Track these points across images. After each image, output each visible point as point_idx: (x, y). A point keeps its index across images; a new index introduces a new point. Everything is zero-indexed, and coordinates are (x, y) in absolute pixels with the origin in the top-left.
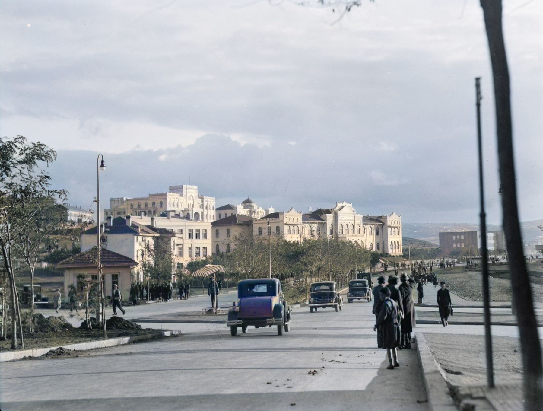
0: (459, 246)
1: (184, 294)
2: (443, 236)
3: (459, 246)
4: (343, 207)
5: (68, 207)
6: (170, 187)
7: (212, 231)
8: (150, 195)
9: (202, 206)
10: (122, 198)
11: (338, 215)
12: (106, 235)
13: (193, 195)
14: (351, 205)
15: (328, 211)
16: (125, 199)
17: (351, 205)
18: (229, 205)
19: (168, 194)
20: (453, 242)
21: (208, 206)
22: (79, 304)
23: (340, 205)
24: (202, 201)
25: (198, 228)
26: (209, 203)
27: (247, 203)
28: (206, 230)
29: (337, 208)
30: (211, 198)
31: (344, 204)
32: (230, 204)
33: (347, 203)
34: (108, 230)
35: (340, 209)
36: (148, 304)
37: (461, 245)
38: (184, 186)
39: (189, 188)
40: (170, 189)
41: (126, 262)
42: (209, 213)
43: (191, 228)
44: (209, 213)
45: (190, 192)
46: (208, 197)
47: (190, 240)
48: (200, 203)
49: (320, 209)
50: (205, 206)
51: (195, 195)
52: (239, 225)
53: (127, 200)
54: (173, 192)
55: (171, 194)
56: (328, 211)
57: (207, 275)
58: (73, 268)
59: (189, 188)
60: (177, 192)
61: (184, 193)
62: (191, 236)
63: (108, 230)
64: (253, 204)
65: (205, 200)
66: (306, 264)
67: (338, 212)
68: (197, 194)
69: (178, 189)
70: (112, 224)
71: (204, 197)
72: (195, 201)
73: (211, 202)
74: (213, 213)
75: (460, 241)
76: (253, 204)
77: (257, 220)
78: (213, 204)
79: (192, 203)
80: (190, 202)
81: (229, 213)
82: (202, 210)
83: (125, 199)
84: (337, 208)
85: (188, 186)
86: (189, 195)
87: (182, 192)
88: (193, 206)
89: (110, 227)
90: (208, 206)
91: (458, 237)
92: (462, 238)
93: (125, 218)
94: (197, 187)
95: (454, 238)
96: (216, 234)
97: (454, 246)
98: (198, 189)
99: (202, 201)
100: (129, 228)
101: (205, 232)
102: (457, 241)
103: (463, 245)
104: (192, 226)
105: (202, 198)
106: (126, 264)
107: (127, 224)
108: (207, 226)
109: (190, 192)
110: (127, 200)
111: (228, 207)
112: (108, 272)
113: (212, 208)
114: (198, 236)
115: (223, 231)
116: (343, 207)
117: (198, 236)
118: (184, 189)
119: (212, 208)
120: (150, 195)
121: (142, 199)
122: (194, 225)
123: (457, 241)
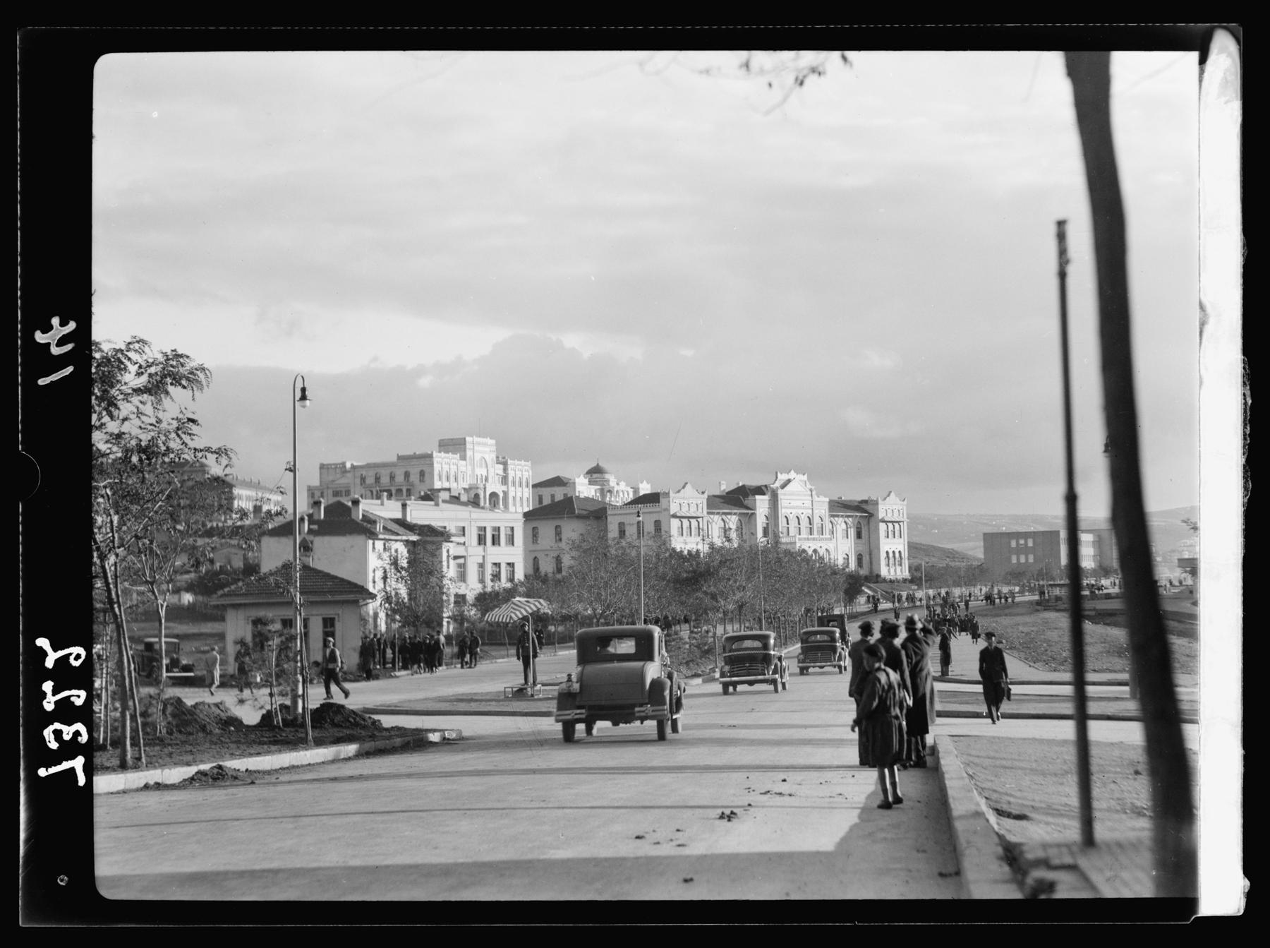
1: (467, 658)
2: (994, 540)
3: (1023, 560)
4: (789, 481)
5: (234, 482)
8: (399, 458)
9: (504, 480)
10: (344, 464)
11: (780, 497)
12: (310, 538)
13: (487, 457)
14: (805, 477)
15: (760, 490)
17: (805, 477)
18: (558, 478)
19: (435, 454)
20: (1011, 551)
23: (783, 477)
24: (505, 470)
26: (519, 474)
27: (596, 473)
29: (777, 484)
30: (523, 463)
31: (792, 475)
32: (561, 475)
34: (315, 527)
35: (783, 487)
37: (1018, 559)
39: (479, 444)
41: (351, 592)
42: (519, 494)
43: (483, 525)
44: (519, 494)
47: (481, 548)
48: (501, 472)
50: (510, 479)
51: (491, 457)
52: (579, 517)
54: (447, 452)
55: (443, 454)
56: (760, 490)
59: (479, 444)
60: (454, 452)
61: (469, 453)
62: (481, 540)
63: (315, 527)
64: (607, 476)
65: (510, 467)
67: (780, 491)
68: (494, 456)
69: (455, 445)
72: (491, 470)
73: (522, 471)
74: (527, 493)
75: (1026, 550)
76: (607, 476)
77: (615, 507)
78: (526, 475)
79: (484, 474)
80: (481, 472)
81: (559, 494)
82: (504, 488)
83: (348, 465)
85: (477, 439)
86: (478, 457)
87: (465, 450)
88: (487, 480)
89: (318, 522)
91: (1022, 542)
92: (1030, 544)
93: (350, 504)
94: (493, 442)
95: (1013, 544)
96: (534, 535)
97: (1014, 560)
98: (497, 444)
99: (505, 470)
102: (1018, 551)
104: (485, 520)
105: (505, 464)
107: (353, 516)
111: (557, 482)
114: (496, 541)
116: (789, 481)
118: (468, 446)
120: (399, 458)
121: (384, 465)
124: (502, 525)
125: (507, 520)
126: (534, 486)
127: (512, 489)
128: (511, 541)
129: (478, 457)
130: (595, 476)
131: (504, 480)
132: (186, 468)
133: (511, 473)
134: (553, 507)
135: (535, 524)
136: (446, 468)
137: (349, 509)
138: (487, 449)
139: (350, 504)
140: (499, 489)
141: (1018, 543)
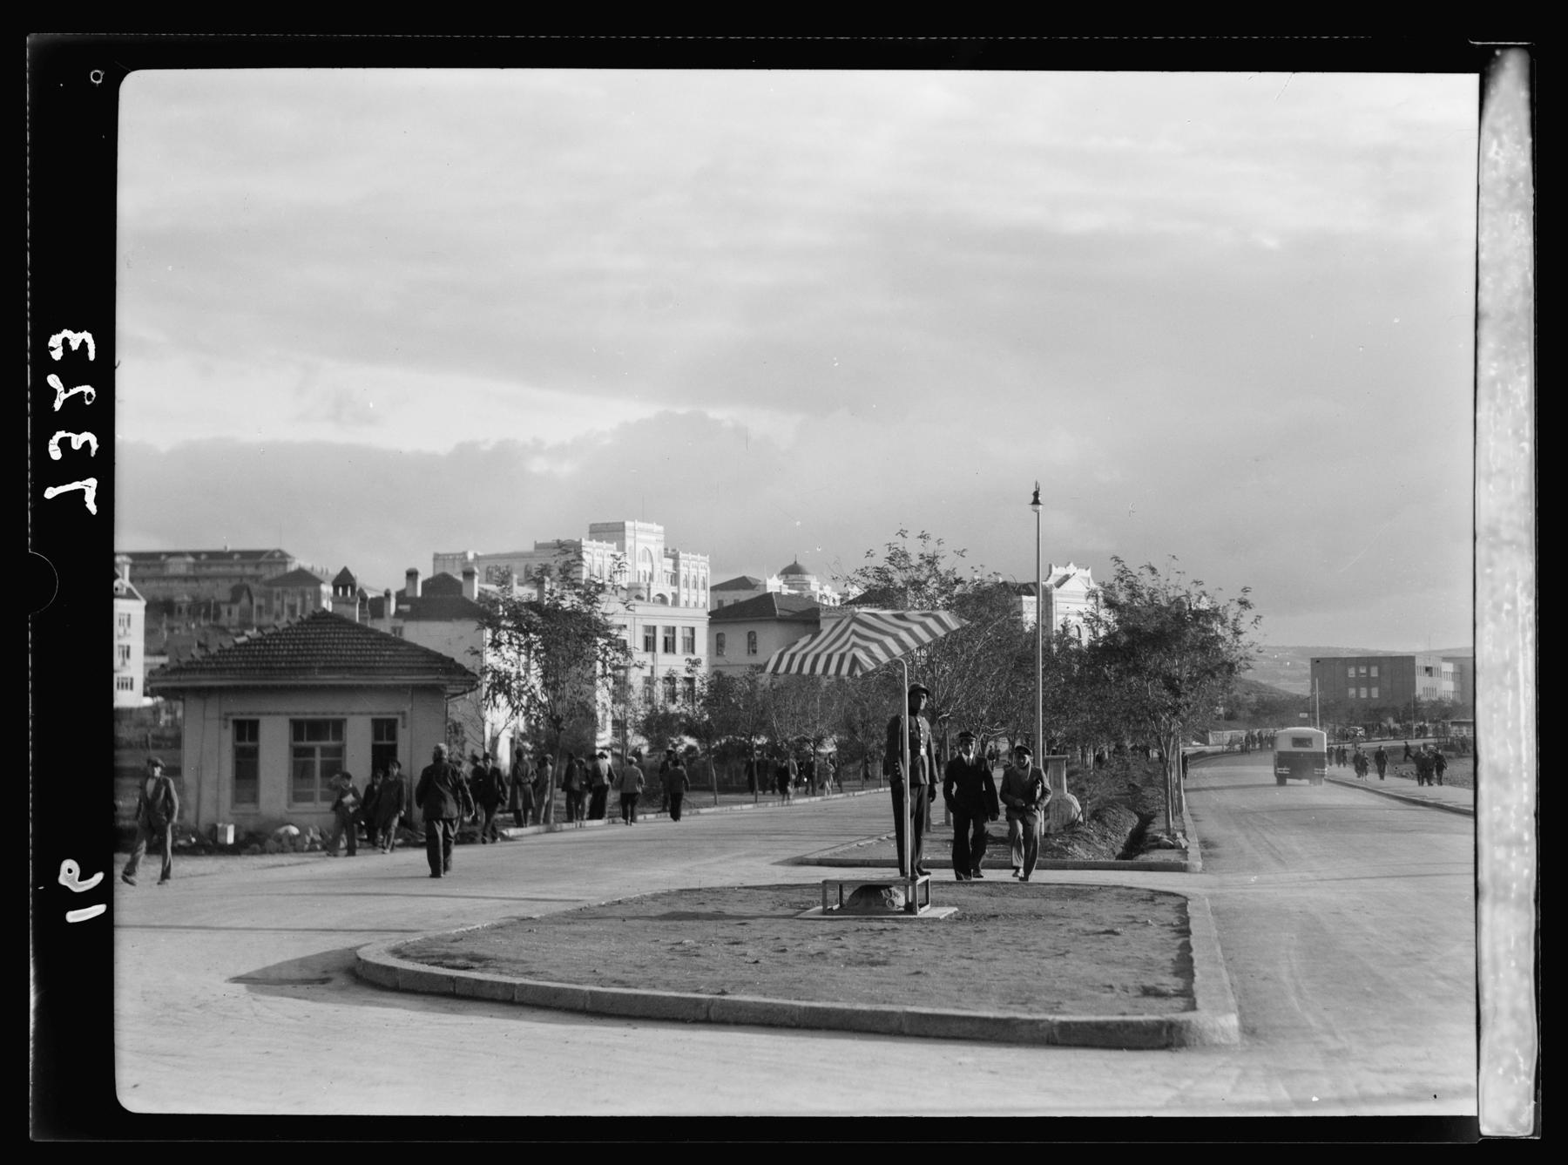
0: (1363, 695)
1: (1180, 667)
2: (1323, 666)
4: (1067, 578)
5: (322, 577)
6: (592, 526)
7: (709, 636)
9: (675, 579)
10: (465, 554)
11: (1055, 599)
12: (400, 623)
13: (652, 548)
14: (1088, 573)
15: (1028, 589)
16: (471, 556)
17: (1088, 573)
18: (744, 579)
19: (584, 542)
21: (691, 579)
22: (225, 832)
23: (1058, 572)
24: (676, 566)
25: (671, 623)
26: (693, 572)
28: (693, 630)
29: (1052, 581)
30: (699, 557)
31: (1071, 569)
32: (747, 575)
33: (1079, 566)
34: (406, 608)
35: (1059, 585)
36: (505, 838)
37: (1369, 693)
38: (628, 524)
39: (642, 530)
40: (591, 532)
41: (429, 670)
43: (651, 623)
44: (693, 599)
45: (643, 541)
46: (690, 556)
48: (670, 569)
49: (1005, 583)
51: (657, 548)
52: (782, 620)
53: (477, 558)
54: (600, 540)
55: (594, 543)
56: (1028, 589)
57: (870, 665)
58: (221, 691)
59: (642, 530)
60: (609, 541)
61: (629, 543)
62: (649, 644)
63: (406, 608)
64: (807, 578)
65: (682, 562)
66: (1171, 685)
67: (1055, 591)
68: (661, 547)
69: (611, 532)
70: (419, 594)
71: (681, 555)
72: (658, 566)
73: (697, 568)
75: (1368, 682)
76: (807, 578)
77: (829, 609)
78: (703, 573)
79: (649, 570)
80: (644, 567)
81: (744, 596)
82: (674, 589)
83: (471, 556)
84: (1052, 581)
85: (639, 525)
86: (640, 547)
87: (623, 538)
88: (651, 578)
89: (413, 601)
90: (691, 579)
91: (1363, 670)
92: (1374, 672)
93: (460, 578)
94: (661, 528)
95: (1352, 672)
96: (718, 645)
97: (1352, 692)
98: (665, 533)
99: (676, 566)
100: (471, 604)
101: (688, 635)
102: (1360, 682)
103: (1375, 693)
105: (676, 558)
106: (429, 679)
107: (465, 594)
108: (697, 618)
109: (643, 541)
110: (477, 558)
111: (743, 583)
112: (356, 709)
113: (700, 585)
114: (669, 646)
115: (736, 637)
116: (1067, 578)
117: (669, 646)
118: (628, 533)
119: (700, 585)
122: (661, 618)
123: (1360, 682)
124: (679, 625)
125: (684, 618)
126: (713, 589)
127: (684, 591)
128: (690, 645)
129: (640, 547)
130: (792, 577)
131: (675, 579)
132: (262, 559)
133: (683, 570)
134: (740, 610)
135: (719, 629)
136: (598, 560)
137: (459, 585)
138: (653, 538)
139: (460, 578)
140: (668, 590)
141: (1357, 673)
